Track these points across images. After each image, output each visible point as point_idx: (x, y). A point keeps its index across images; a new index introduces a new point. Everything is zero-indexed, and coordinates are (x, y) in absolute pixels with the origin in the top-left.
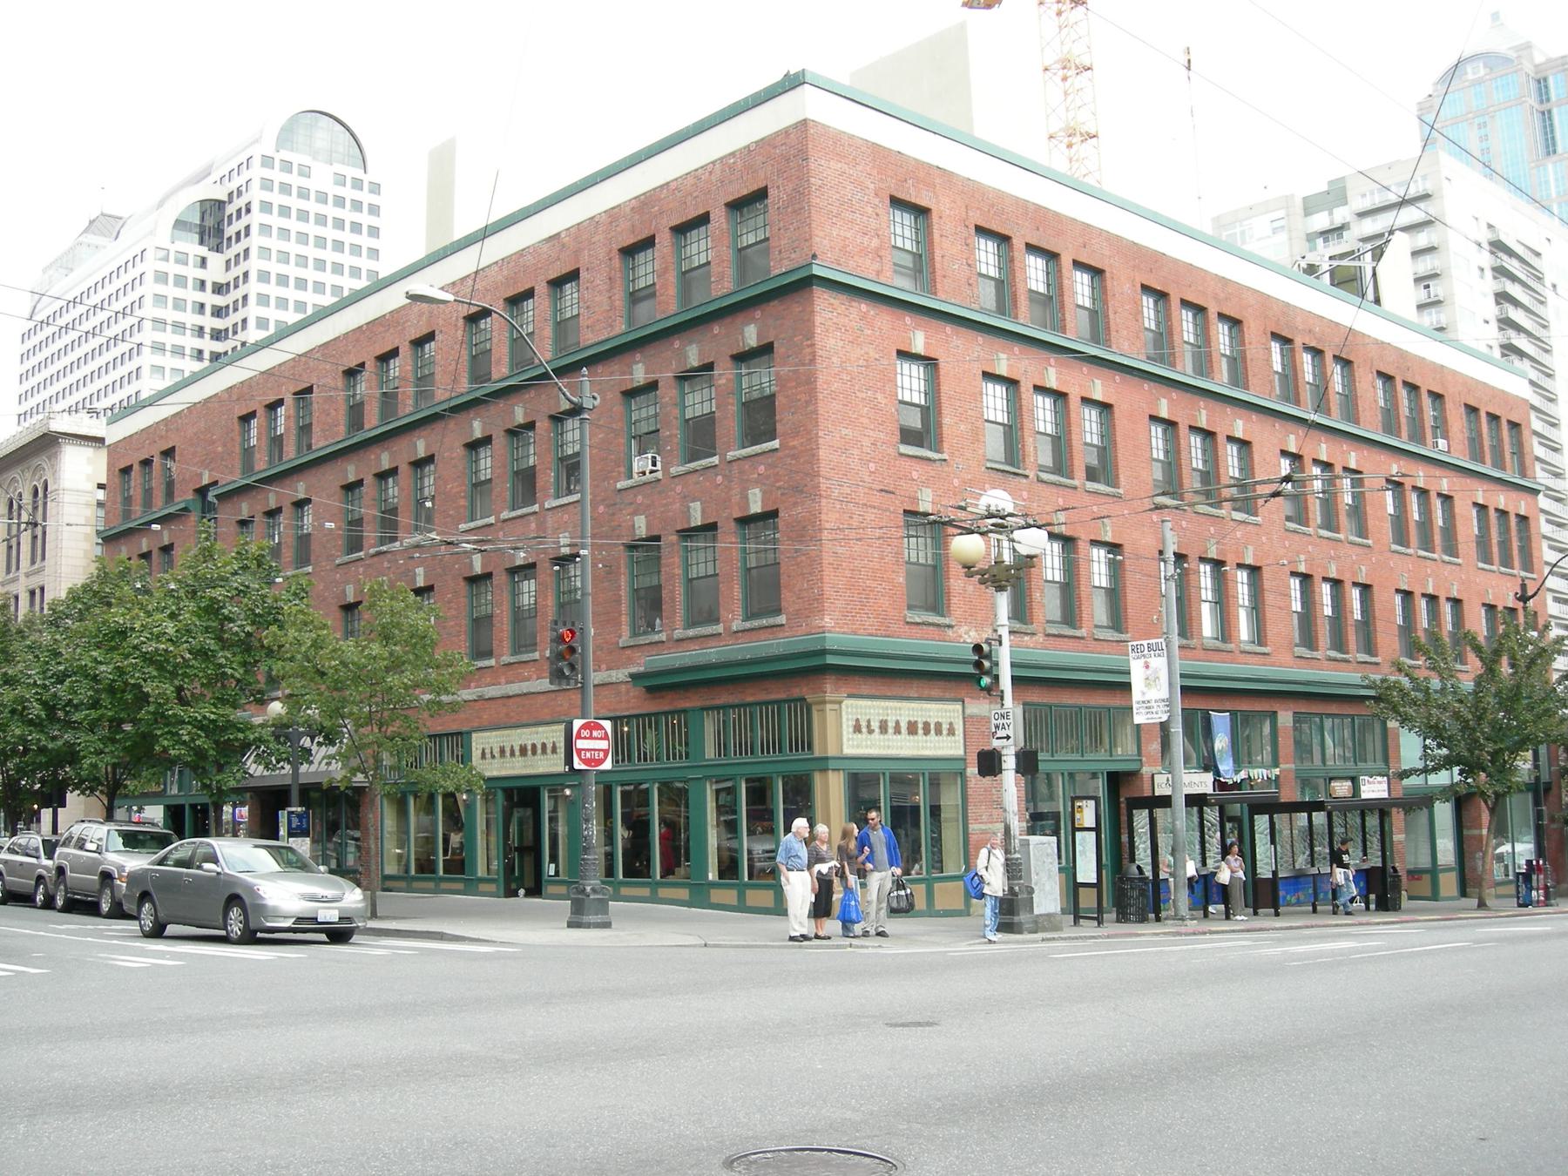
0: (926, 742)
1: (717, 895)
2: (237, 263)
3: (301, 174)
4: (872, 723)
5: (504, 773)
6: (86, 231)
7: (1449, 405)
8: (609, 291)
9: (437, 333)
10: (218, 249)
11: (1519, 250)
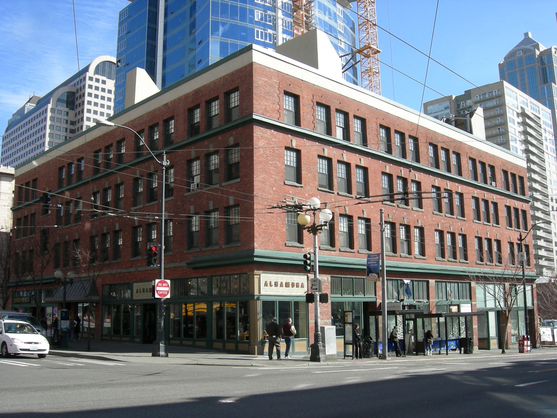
0: (293, 290)
1: (216, 345)
2: (79, 114)
4: (272, 283)
5: (141, 298)
6: (28, 102)
9: (126, 138)
10: (72, 109)
11: (532, 116)
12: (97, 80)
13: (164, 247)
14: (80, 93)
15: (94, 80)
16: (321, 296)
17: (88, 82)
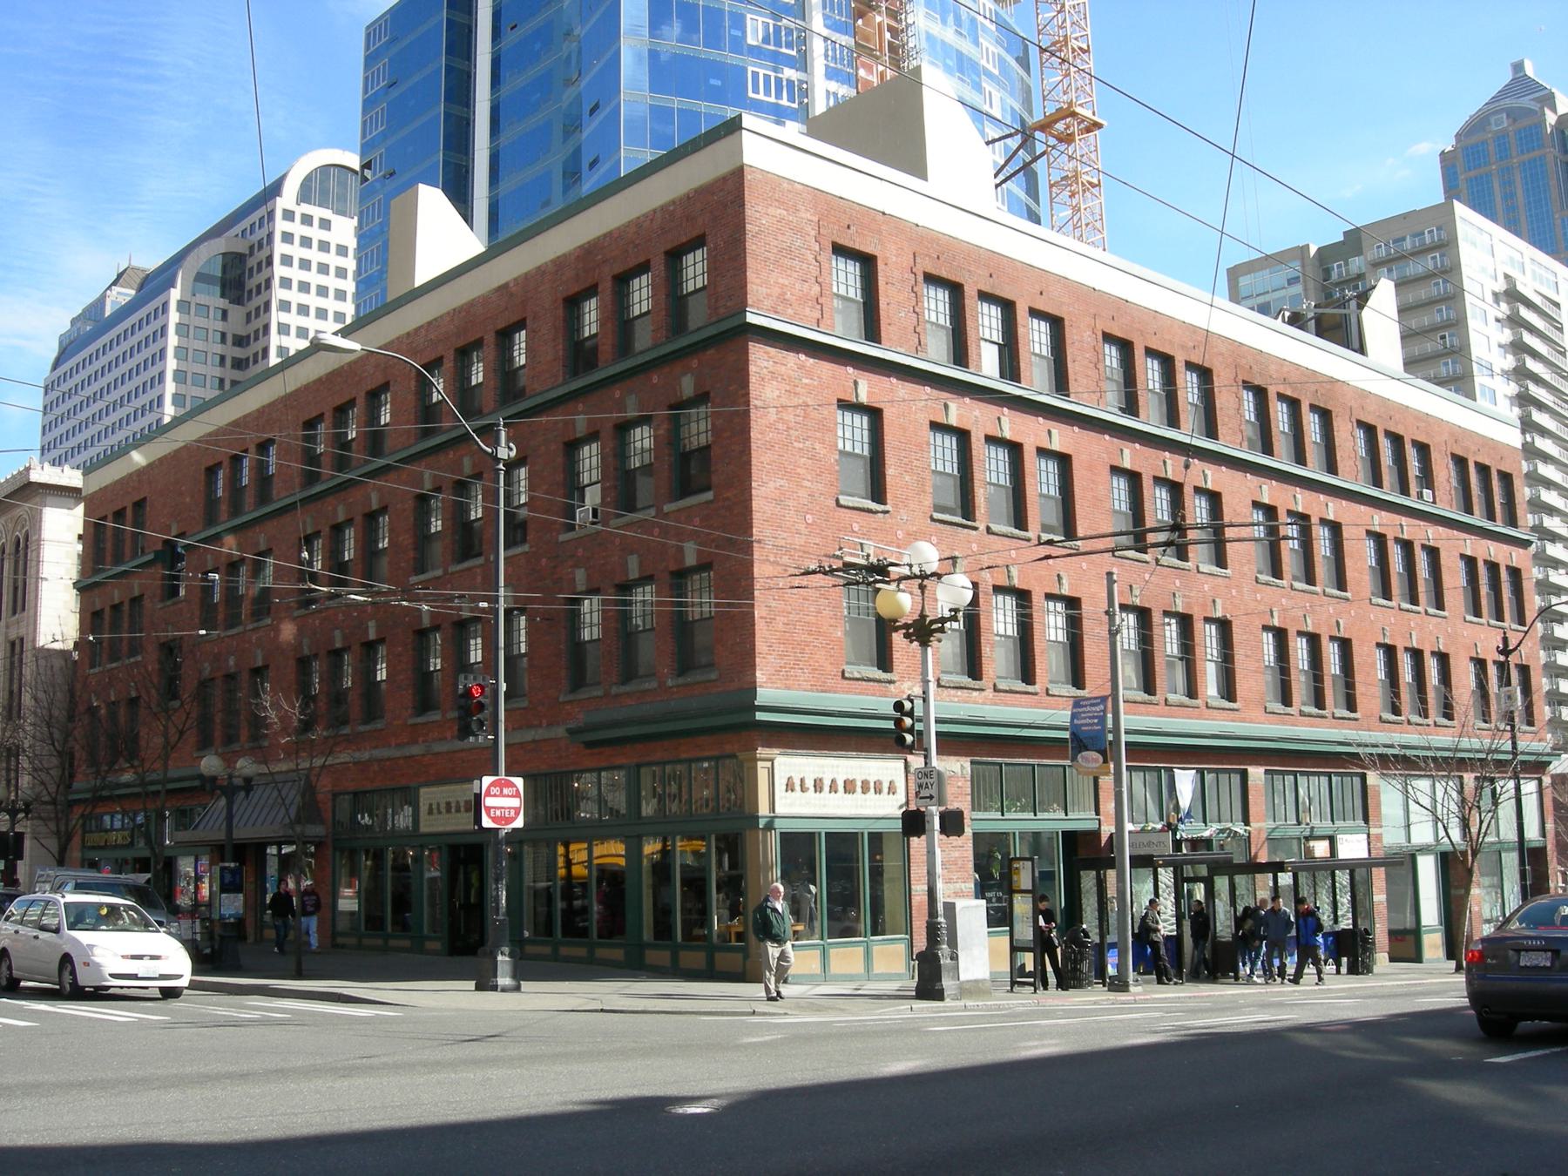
2: (257, 315)
3: (321, 227)
5: (449, 828)
6: (115, 283)
7: (1434, 455)
8: (554, 340)
9: (391, 383)
10: (238, 301)
11: (1537, 300)
12: (307, 220)
13: (503, 687)
14: (262, 255)
15: (298, 218)
16: (943, 816)
17: (281, 225)
